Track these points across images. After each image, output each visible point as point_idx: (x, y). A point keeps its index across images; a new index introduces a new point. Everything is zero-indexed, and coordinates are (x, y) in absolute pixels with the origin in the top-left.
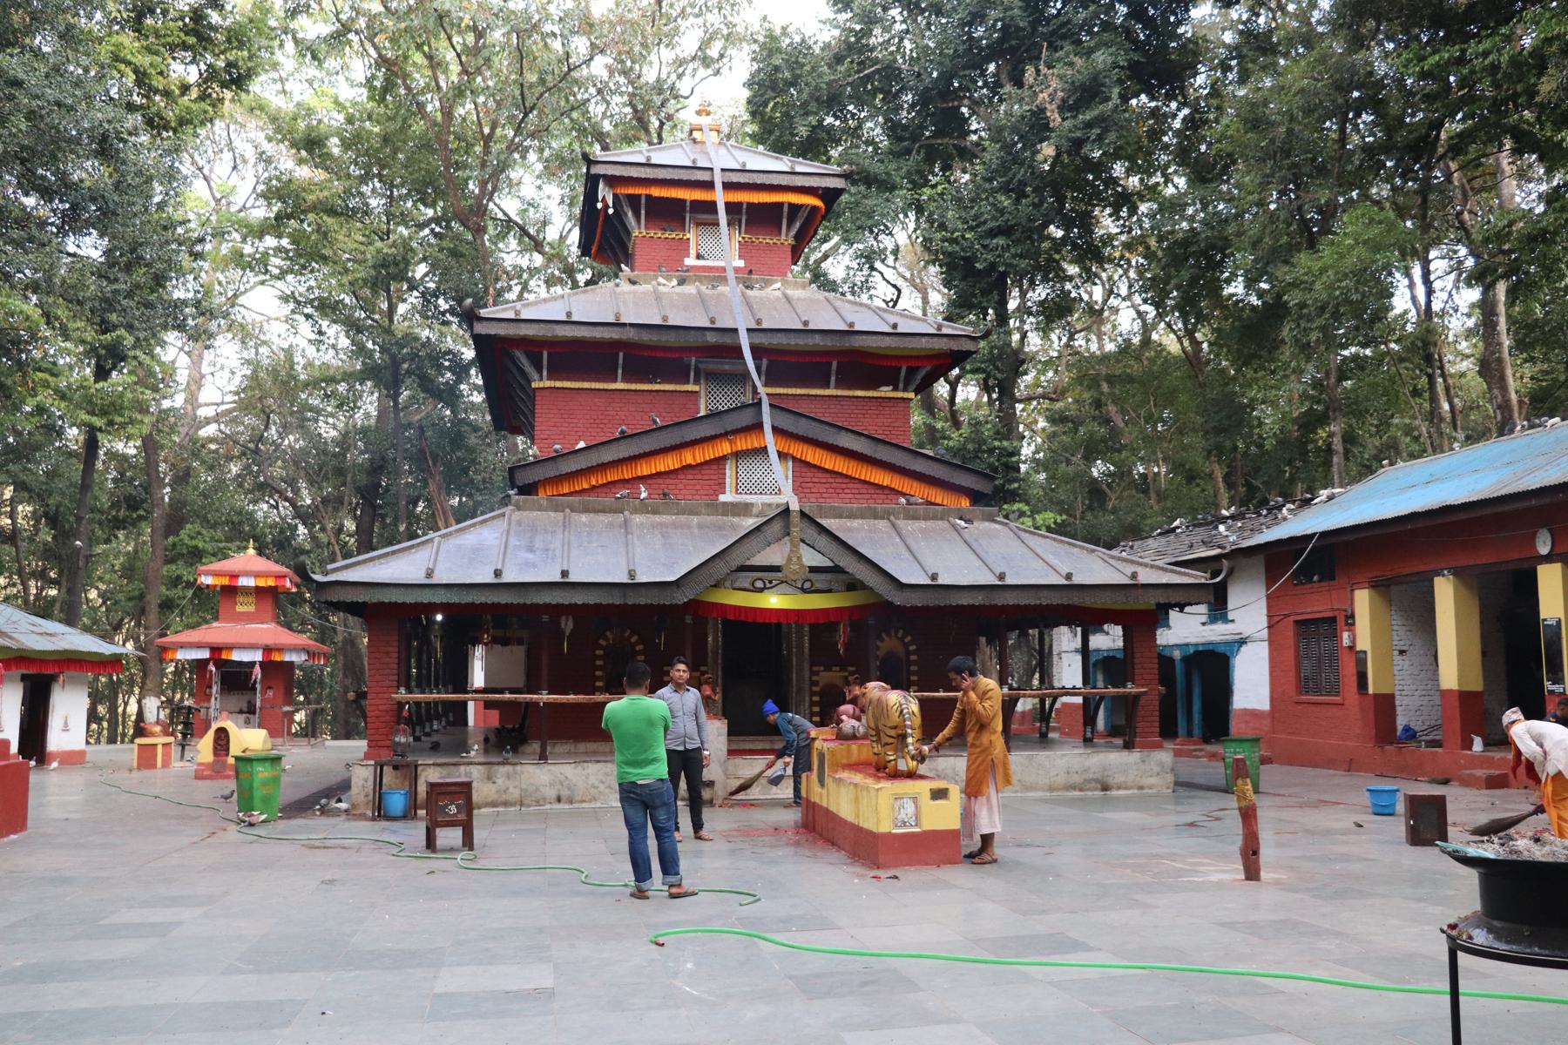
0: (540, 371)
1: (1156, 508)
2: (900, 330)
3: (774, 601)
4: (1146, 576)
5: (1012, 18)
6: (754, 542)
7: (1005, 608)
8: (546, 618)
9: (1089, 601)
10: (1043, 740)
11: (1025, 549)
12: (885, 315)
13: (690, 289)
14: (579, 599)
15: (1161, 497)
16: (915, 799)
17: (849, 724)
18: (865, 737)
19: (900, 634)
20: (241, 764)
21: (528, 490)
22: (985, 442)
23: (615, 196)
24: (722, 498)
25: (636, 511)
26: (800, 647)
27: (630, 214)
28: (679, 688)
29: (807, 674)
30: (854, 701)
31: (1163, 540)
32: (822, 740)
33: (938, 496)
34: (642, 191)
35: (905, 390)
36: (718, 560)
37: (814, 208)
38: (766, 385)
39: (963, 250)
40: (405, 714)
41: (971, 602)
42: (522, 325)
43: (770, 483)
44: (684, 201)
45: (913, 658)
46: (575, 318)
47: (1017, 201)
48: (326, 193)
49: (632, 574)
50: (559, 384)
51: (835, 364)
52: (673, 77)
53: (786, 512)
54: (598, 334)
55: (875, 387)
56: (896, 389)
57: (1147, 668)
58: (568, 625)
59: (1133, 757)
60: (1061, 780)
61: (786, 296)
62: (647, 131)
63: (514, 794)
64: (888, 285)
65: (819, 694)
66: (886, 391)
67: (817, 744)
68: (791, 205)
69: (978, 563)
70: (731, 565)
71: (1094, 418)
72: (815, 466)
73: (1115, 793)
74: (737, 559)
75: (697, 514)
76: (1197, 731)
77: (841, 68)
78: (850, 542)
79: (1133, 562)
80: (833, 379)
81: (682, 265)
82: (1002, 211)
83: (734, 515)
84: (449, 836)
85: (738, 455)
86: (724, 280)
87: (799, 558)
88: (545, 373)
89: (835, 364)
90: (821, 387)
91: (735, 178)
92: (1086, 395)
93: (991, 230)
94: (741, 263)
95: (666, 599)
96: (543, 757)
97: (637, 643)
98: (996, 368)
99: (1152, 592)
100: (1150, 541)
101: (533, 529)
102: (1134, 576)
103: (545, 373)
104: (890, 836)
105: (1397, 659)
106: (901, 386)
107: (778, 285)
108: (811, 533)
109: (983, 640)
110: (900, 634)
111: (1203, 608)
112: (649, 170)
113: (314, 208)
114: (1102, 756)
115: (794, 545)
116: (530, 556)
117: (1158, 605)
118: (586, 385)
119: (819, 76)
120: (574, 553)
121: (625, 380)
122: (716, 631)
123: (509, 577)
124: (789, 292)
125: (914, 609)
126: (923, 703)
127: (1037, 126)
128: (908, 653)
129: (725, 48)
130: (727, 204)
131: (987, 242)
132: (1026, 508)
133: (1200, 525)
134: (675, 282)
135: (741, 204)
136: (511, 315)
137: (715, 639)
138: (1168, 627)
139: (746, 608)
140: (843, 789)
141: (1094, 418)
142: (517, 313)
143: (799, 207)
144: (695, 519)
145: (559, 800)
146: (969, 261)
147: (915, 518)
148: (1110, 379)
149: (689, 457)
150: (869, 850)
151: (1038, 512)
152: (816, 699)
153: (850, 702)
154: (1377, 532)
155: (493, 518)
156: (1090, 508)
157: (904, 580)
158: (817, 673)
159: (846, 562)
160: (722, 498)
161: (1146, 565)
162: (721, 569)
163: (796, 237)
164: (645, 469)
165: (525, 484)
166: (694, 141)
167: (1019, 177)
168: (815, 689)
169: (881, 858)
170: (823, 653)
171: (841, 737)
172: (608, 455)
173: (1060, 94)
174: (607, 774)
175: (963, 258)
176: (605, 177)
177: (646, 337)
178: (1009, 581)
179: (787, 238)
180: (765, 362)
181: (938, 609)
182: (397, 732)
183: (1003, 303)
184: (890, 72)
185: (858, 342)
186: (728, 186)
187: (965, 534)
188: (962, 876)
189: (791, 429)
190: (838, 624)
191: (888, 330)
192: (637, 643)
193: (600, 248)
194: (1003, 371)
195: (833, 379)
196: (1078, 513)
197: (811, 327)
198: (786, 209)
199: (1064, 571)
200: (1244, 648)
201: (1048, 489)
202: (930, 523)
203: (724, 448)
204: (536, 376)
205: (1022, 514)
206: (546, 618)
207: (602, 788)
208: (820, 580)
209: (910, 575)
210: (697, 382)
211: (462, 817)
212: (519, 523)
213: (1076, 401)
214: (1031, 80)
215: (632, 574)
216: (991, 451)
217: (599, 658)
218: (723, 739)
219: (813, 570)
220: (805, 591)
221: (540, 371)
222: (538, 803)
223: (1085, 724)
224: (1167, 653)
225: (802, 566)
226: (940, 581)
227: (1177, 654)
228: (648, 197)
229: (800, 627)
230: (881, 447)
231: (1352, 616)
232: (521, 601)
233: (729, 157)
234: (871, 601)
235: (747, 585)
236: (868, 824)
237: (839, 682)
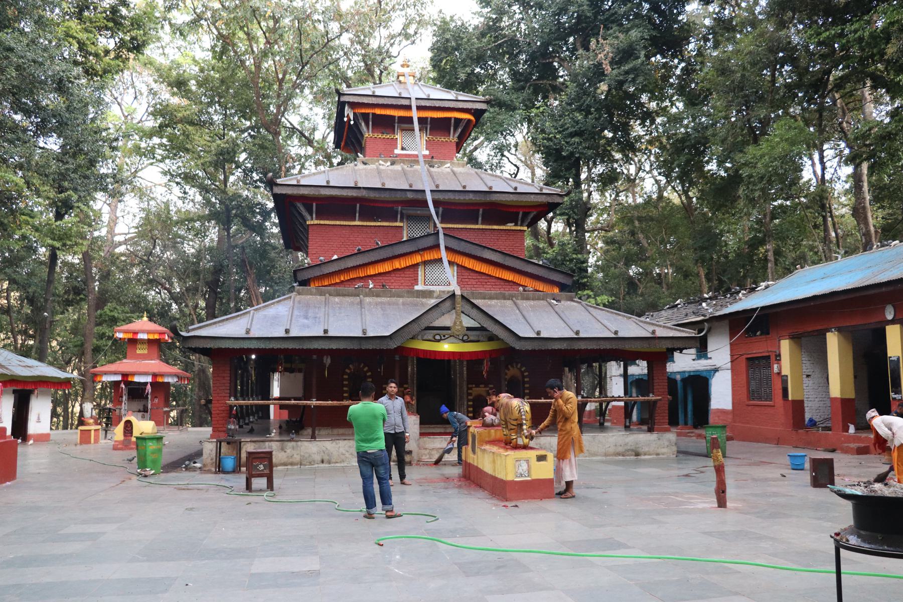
0: (311, 215)
2: (518, 191)
3: (446, 347)
4: (661, 333)
5: (583, 11)
6: (434, 313)
7: (579, 350)
9: (628, 347)
10: (601, 427)
11: (591, 317)
12: (510, 182)
13: (398, 167)
14: (334, 346)
16: (527, 461)
17: (489, 418)
18: (498, 425)
19: (519, 366)
20: (139, 441)
21: (304, 283)
22: (567, 255)
23: (355, 114)
24: (416, 288)
25: (366, 295)
26: (461, 373)
27: (363, 124)
28: (391, 397)
29: (465, 389)
30: (492, 405)
31: (670, 312)
32: (474, 427)
33: (541, 286)
35: (521, 225)
37: (469, 120)
38: (441, 222)
40: (234, 412)
42: (301, 188)
43: (444, 279)
46: (331, 184)
47: (586, 117)
48: (188, 112)
49: (364, 332)
50: (322, 222)
51: (481, 212)
52: (388, 45)
54: (345, 193)
55: (504, 224)
56: (516, 225)
57: (661, 385)
58: (327, 361)
59: (653, 436)
60: (611, 450)
61: (452, 171)
62: (373, 76)
63: (297, 458)
64: (511, 165)
65: (472, 400)
66: (510, 226)
67: (471, 430)
68: (455, 118)
69: (564, 325)
70: (421, 327)
71: (630, 241)
72: (470, 269)
73: (643, 457)
74: (424, 323)
76: (690, 422)
78: (490, 313)
79: (653, 324)
80: (480, 219)
81: (393, 153)
82: (577, 122)
83: (423, 297)
84: (259, 483)
85: (425, 263)
86: (417, 162)
87: (461, 322)
88: (314, 216)
89: (481, 212)
90: (473, 223)
91: (423, 103)
92: (626, 228)
94: (427, 153)
96: (313, 437)
97: (367, 371)
98: (574, 212)
99: (663, 342)
100: (663, 312)
101: (308, 306)
102: (654, 332)
103: (314, 216)
104: (513, 482)
105: (805, 380)
106: (519, 223)
107: (448, 165)
108: (467, 308)
109: (567, 369)
110: (519, 366)
111: (693, 351)
112: (374, 99)
113: (181, 121)
114: (635, 436)
116: (306, 321)
117: (668, 349)
118: (338, 223)
120: (331, 319)
121: (360, 220)
122: (413, 365)
123: (294, 333)
124: (455, 169)
126: (532, 406)
127: (598, 73)
128: (524, 377)
129: (418, 28)
130: (419, 118)
131: (568, 140)
132: (591, 293)
133: (691, 303)
134: (389, 163)
135: (427, 118)
136: (295, 183)
137: (413, 369)
138: (673, 361)
139: (427, 351)
140: (486, 456)
141: (630, 241)
142: (298, 181)
144: (401, 300)
145: (323, 462)
146: (559, 151)
147: (528, 299)
148: (640, 219)
149: (397, 264)
150: (501, 491)
151: (599, 296)
152: (471, 403)
153: (490, 405)
154: (774, 310)
155: (285, 299)
156: (628, 293)
157: (521, 335)
158: (471, 389)
160: (416, 288)
161: (660, 326)
162: (416, 328)
163: (459, 137)
164: (371, 271)
165: (303, 279)
166: (400, 82)
167: (587, 102)
168: (470, 397)
169: (508, 495)
170: (475, 378)
171: (485, 425)
172: (350, 263)
173: (611, 55)
174: (350, 447)
175: (555, 149)
176: (349, 103)
177: (372, 195)
178: (582, 335)
179: (453, 138)
180: (441, 209)
181: (541, 351)
182: (229, 423)
183: (578, 175)
184: (512, 42)
185: (495, 198)
186: (419, 108)
187: (556, 308)
188: (555, 505)
189: (456, 248)
190: (483, 360)
191: (512, 190)
192: (367, 371)
193: (346, 143)
194: (578, 214)
195: (480, 219)
197: (467, 189)
198: (453, 121)
199: (614, 329)
200: (717, 374)
201: (604, 283)
202: (536, 302)
203: (418, 259)
204: (309, 217)
205: (589, 297)
206: (315, 357)
207: (347, 455)
208: (473, 335)
209: (525, 331)
210: (402, 221)
211: (267, 471)
212: (299, 302)
213: (620, 231)
216: (571, 260)
217: (346, 380)
218: (417, 426)
219: (469, 329)
220: (464, 341)
221: (311, 215)
222: (310, 463)
223: (626, 418)
224: (673, 377)
225: (462, 327)
226: (542, 335)
227: (678, 377)
228: (374, 114)
229: (461, 363)
230: (508, 258)
231: (779, 355)
232: (301, 347)
233: (420, 92)
234: (502, 347)
235: (431, 338)
236: (501, 475)
237: (484, 394)
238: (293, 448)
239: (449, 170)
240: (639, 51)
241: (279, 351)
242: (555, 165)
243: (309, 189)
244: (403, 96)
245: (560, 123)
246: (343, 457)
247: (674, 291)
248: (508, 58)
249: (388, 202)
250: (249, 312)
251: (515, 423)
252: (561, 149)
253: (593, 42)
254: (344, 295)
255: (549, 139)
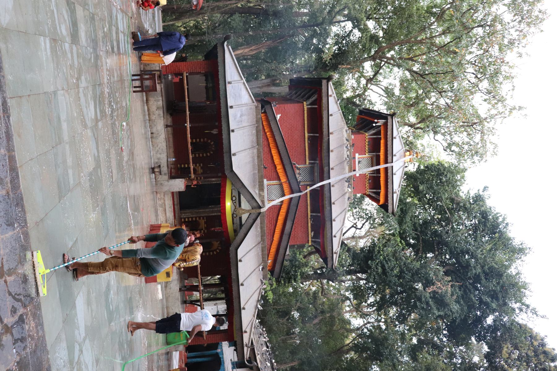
1: (279, 339)
2: (334, 239)
3: (228, 204)
5: (471, 270)
7: (231, 287)
8: (217, 124)
12: (340, 232)
14: (224, 136)
15: (284, 341)
23: (380, 126)
24: (265, 180)
26: (213, 212)
27: (374, 132)
34: (382, 136)
35: (312, 241)
36: (241, 184)
39: (376, 255)
41: (233, 274)
43: (272, 198)
44: (380, 152)
45: (211, 253)
46: (330, 117)
47: (396, 276)
49: (234, 155)
50: (306, 112)
51: (319, 214)
53: (260, 207)
54: (325, 126)
58: (215, 132)
61: (346, 193)
62: (419, 123)
63: (153, 117)
65: (196, 220)
66: (311, 234)
68: (380, 192)
70: (240, 188)
75: (259, 172)
76: (189, 360)
77: (448, 202)
79: (251, 331)
80: (314, 214)
82: (392, 270)
83: (259, 185)
85: (281, 185)
86: (350, 171)
87: (244, 213)
88: (309, 106)
89: (319, 214)
90: (311, 210)
91: (390, 171)
92: (326, 307)
93: (385, 266)
95: (226, 167)
96: (167, 126)
98: (329, 272)
102: (246, 332)
103: (309, 106)
106: (313, 240)
107: (350, 190)
108: (253, 216)
111: (236, 359)
112: (391, 138)
115: (248, 211)
116: (239, 115)
117: (236, 342)
118: (306, 122)
119: (444, 193)
122: (216, 181)
123: (230, 110)
125: (229, 255)
126: (197, 266)
127: (428, 283)
130: (379, 169)
136: (330, 93)
137: (214, 181)
138: (230, 346)
139: (225, 191)
142: (331, 96)
143: (379, 195)
145: (152, 133)
149: (279, 167)
152: (194, 219)
156: (278, 312)
157: (239, 250)
158: (203, 219)
159: (244, 229)
160: (265, 180)
161: (250, 336)
168: (198, 219)
173: (440, 291)
174: (162, 150)
175: (372, 255)
178: (241, 288)
180: (319, 189)
181: (229, 262)
184: (448, 221)
187: (257, 270)
191: (333, 234)
193: (362, 119)
194: (331, 275)
195: (314, 214)
196: (275, 307)
197: (333, 206)
201: (285, 294)
203: (283, 179)
204: (308, 103)
205: (271, 285)
208: (237, 220)
209: (241, 252)
210: (310, 163)
213: (324, 302)
214: (446, 279)
215: (234, 155)
216: (296, 271)
218: (178, 190)
219: (240, 218)
220: (233, 215)
221: (310, 105)
222: (150, 126)
224: (219, 347)
226: (239, 263)
227: (219, 351)
228: (380, 139)
229: (219, 211)
230: (288, 236)
232: (222, 116)
237: (200, 227)
238: (159, 115)
239: (346, 190)
240: (443, 311)
241: (219, 103)
242: (362, 255)
243: (326, 104)
244: (394, 157)
245: (391, 258)
246: (156, 146)
247: (282, 345)
248: (438, 218)
249: (321, 154)
250: (242, 79)
251: (187, 258)
252: (372, 260)
253: (449, 278)
254: (257, 135)
255: (379, 252)
